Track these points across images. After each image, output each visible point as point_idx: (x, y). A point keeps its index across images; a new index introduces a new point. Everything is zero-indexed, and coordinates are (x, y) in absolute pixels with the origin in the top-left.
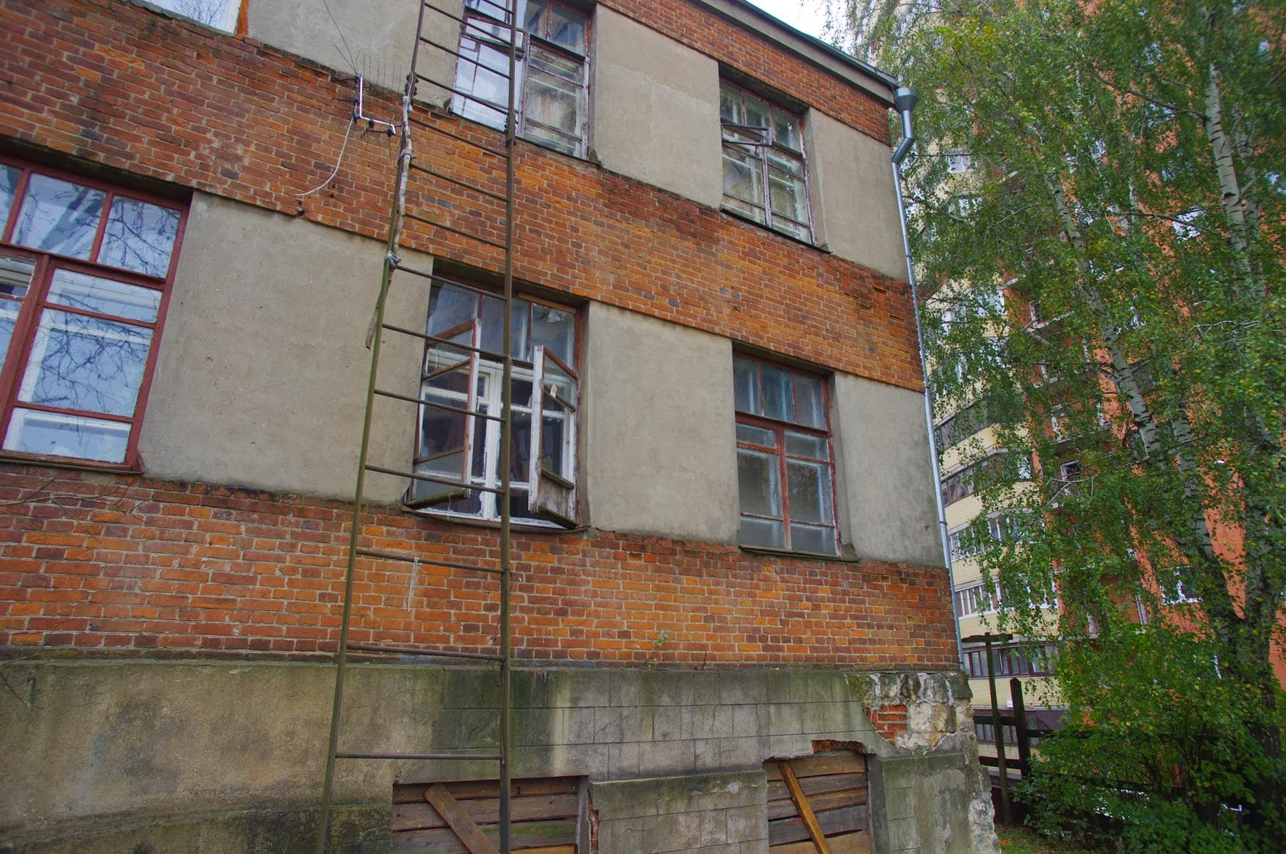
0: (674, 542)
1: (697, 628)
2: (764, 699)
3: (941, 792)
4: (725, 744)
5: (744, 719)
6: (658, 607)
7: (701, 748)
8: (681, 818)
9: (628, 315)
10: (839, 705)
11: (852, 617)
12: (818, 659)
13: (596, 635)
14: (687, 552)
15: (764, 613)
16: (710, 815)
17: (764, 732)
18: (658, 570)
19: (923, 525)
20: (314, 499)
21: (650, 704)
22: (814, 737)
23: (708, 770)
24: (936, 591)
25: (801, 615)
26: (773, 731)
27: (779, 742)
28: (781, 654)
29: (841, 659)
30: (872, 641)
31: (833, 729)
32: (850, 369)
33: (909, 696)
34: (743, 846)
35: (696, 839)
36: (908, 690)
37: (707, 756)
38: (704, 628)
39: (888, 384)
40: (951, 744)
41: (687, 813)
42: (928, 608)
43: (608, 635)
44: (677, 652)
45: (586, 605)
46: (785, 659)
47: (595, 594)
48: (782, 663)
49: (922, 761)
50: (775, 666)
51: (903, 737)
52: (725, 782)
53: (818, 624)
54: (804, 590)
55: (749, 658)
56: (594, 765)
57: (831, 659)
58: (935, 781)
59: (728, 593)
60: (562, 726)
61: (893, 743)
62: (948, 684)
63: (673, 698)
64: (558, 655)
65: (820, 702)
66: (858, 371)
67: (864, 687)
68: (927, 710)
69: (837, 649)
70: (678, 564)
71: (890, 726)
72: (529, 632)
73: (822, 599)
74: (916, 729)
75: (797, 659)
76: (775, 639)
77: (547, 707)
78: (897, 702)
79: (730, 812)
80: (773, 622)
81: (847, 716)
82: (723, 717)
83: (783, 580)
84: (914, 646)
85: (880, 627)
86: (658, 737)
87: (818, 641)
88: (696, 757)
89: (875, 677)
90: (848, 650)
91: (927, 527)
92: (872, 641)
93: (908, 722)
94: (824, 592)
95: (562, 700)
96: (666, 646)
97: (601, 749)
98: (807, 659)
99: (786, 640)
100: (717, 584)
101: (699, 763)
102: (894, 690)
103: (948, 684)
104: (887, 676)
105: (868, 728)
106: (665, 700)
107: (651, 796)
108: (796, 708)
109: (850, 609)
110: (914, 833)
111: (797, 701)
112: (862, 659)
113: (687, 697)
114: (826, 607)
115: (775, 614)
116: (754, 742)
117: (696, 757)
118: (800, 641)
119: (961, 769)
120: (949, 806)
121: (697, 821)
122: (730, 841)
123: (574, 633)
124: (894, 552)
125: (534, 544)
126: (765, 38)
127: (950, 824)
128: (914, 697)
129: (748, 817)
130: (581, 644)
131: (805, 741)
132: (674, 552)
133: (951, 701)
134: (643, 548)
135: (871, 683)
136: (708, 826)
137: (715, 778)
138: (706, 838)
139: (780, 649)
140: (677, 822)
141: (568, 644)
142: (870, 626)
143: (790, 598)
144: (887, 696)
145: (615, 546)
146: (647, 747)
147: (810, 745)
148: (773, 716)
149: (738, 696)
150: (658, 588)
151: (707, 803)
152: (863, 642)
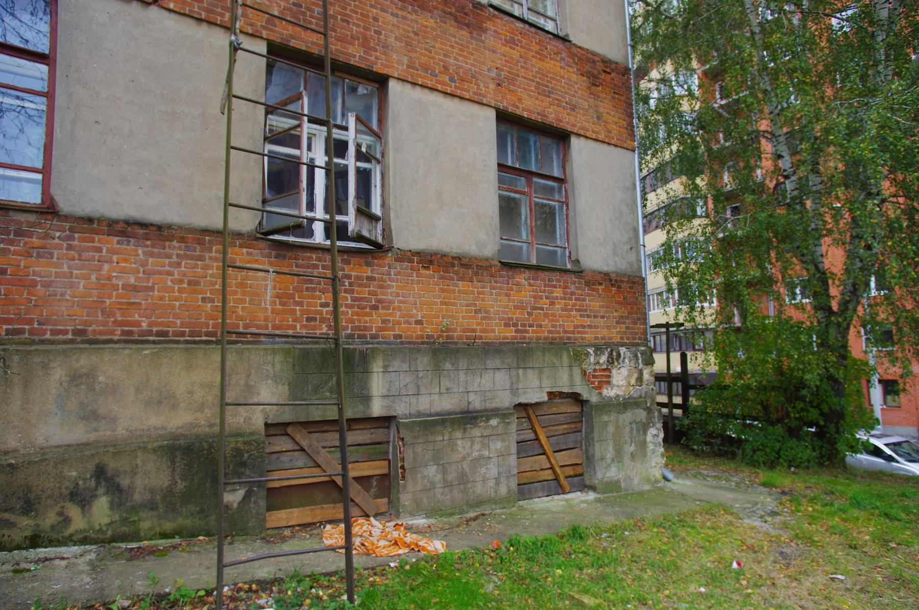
1: (470, 318)
2: (515, 365)
3: (631, 423)
4: (488, 394)
5: (502, 379)
6: (442, 303)
7: (472, 397)
8: (459, 442)
10: (566, 369)
11: (577, 310)
12: (553, 339)
13: (399, 323)
14: (462, 265)
18: (442, 278)
21: (437, 369)
25: (542, 309)
26: (521, 386)
27: (525, 393)
28: (527, 335)
29: (568, 338)
30: (590, 327)
31: (561, 384)
33: (613, 363)
34: (500, 458)
35: (469, 454)
36: (612, 359)
37: (476, 403)
42: (629, 304)
44: (455, 334)
45: (391, 302)
46: (530, 338)
48: (527, 341)
49: (619, 404)
50: (523, 343)
51: (607, 389)
52: (488, 419)
53: (553, 315)
54: (544, 291)
55: (505, 338)
56: (400, 409)
57: (561, 338)
58: (627, 416)
60: (378, 384)
61: (600, 393)
62: (639, 355)
65: (553, 366)
69: (566, 332)
70: (456, 273)
71: (599, 382)
73: (557, 298)
74: (617, 384)
75: (538, 338)
77: (367, 371)
78: (605, 367)
79: (491, 438)
80: (522, 313)
83: (530, 285)
85: (595, 317)
88: (469, 403)
89: (591, 351)
90: (573, 332)
92: (590, 327)
93: (611, 379)
94: (558, 292)
95: (377, 367)
96: (448, 330)
97: (405, 399)
98: (545, 338)
99: (531, 326)
100: (484, 287)
101: (471, 408)
102: (603, 359)
103: (639, 355)
104: (599, 350)
105: (584, 383)
107: (439, 428)
108: (536, 371)
111: (537, 366)
112: (582, 338)
113: (463, 364)
115: (523, 308)
117: (469, 403)
118: (541, 326)
119: (644, 409)
120: (635, 432)
121: (469, 444)
122: (491, 456)
123: (383, 321)
124: (608, 265)
128: (616, 364)
129: (503, 440)
131: (542, 392)
132: (453, 265)
133: (641, 366)
134: (431, 262)
135: (588, 354)
136: (477, 447)
137: (481, 417)
138: (475, 454)
139: (527, 332)
140: (456, 445)
141: (380, 329)
142: (588, 316)
143: (535, 297)
144: (598, 363)
145: (411, 261)
146: (436, 397)
149: (497, 362)
150: (443, 291)
151: (476, 432)
152: (584, 327)
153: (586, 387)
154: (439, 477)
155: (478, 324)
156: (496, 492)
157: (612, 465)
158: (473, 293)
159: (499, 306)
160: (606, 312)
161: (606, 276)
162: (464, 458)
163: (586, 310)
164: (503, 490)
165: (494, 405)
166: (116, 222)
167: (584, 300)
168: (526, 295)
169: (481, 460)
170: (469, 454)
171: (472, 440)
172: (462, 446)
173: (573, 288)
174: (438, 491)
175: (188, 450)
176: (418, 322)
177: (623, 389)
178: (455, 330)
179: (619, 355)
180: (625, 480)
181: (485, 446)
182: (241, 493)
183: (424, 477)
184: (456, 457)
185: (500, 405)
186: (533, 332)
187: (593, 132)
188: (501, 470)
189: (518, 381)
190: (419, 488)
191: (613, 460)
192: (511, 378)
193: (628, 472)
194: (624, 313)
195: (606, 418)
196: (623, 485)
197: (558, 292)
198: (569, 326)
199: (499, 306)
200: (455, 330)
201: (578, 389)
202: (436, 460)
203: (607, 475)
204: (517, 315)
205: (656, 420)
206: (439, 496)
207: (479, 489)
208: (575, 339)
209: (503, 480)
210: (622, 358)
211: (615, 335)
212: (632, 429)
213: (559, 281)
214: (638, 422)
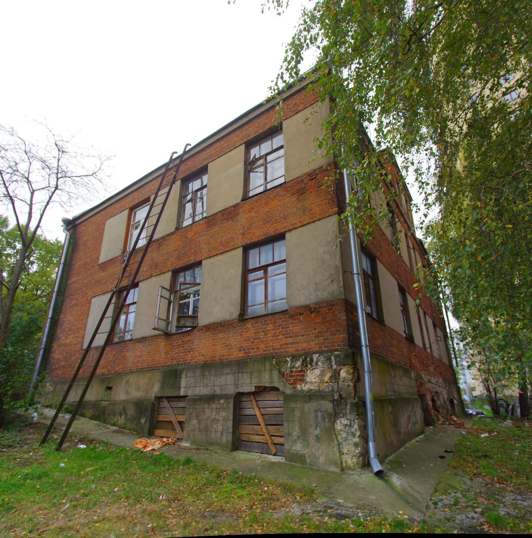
0: (218, 324)
1: (223, 350)
2: (237, 371)
3: (315, 411)
4: (223, 387)
5: (230, 378)
6: (213, 345)
7: (216, 388)
8: (207, 410)
9: (212, 258)
10: (268, 372)
11: (282, 335)
12: (265, 354)
13: (196, 356)
14: (221, 326)
15: (245, 340)
16: (214, 410)
17: (237, 383)
18: (213, 334)
19: (330, 281)
20: (149, 337)
21: (203, 375)
22: (255, 385)
23: (218, 395)
24: (334, 312)
25: (260, 338)
26: (240, 383)
27: (242, 386)
28: (250, 354)
29: (276, 353)
30: (292, 343)
32: (292, 228)
34: (224, 421)
35: (210, 417)
36: (306, 363)
37: (218, 391)
38: (224, 349)
39: (313, 222)
40: (330, 388)
41: (208, 408)
42: (327, 322)
43: (199, 356)
45: (195, 348)
46: (251, 356)
47: (197, 345)
49: (305, 396)
51: (301, 385)
53: (267, 341)
54: (261, 328)
55: (239, 357)
56: (190, 393)
57: (271, 353)
58: (312, 406)
59: (233, 336)
60: (183, 382)
61: (295, 388)
62: (333, 358)
63: (209, 373)
64: (188, 363)
66: (296, 226)
67: (282, 364)
68: (317, 372)
69: (274, 349)
70: (219, 330)
72: (182, 358)
73: (269, 330)
74: (310, 381)
75: (257, 355)
76: (248, 349)
77: (181, 377)
78: (300, 369)
80: (248, 343)
81: (271, 376)
82: (223, 378)
84: (317, 342)
85: (296, 336)
86: (205, 385)
87: (266, 347)
89: (288, 359)
90: (280, 349)
91: (332, 281)
92: (292, 343)
93: (305, 378)
94: (270, 327)
95: (183, 376)
97: (191, 388)
98: (261, 355)
99: (253, 349)
100: (230, 334)
102: (298, 364)
103: (333, 358)
104: (294, 358)
105: (280, 380)
106: (207, 373)
107: (199, 402)
108: (249, 374)
109: (282, 331)
110: (297, 428)
111: (250, 371)
112: (286, 352)
114: (270, 333)
115: (248, 340)
116: (233, 386)
117: (215, 391)
118: (258, 348)
120: (320, 418)
123: (192, 357)
124: (310, 300)
125: (185, 335)
126: (262, 113)
127: (320, 427)
128: (309, 366)
129: (226, 412)
130: (193, 360)
132: (217, 327)
133: (335, 367)
134: (209, 328)
135: (286, 361)
136: (214, 413)
138: (213, 417)
139: (250, 352)
140: (205, 411)
141: (191, 360)
142: (291, 337)
143: (255, 333)
144: (294, 367)
145: (202, 330)
146: (202, 388)
147: (254, 388)
148: (240, 377)
149: (228, 370)
150: (213, 340)
151: (214, 406)
152: (287, 344)
153: (282, 383)
154: (197, 426)
155: (226, 352)
156: (220, 440)
157: (298, 441)
158: (225, 337)
159: (237, 342)
160: (306, 331)
161: (307, 308)
162: (208, 418)
163: (290, 334)
164: (224, 440)
165: (226, 393)
166: (138, 339)
167: (288, 327)
168: (251, 334)
169: (215, 421)
170: (210, 417)
171: (212, 409)
172: (208, 412)
173: (280, 322)
174: (197, 432)
175: (135, 403)
176: (203, 355)
177: (316, 385)
178: (216, 357)
179: (312, 360)
180: (309, 456)
181: (218, 413)
182: (144, 419)
183: (192, 424)
184: (205, 417)
185: (229, 393)
186: (254, 352)
187: (299, 223)
188: (224, 428)
189: (238, 380)
190: (190, 429)
191: (299, 437)
192: (234, 378)
193: (313, 450)
194: (322, 329)
195: (293, 405)
196: (308, 460)
197: (270, 327)
198: (277, 345)
199: (237, 342)
200: (216, 357)
201: (276, 385)
202: (197, 417)
203: (294, 448)
204: (245, 345)
205: (348, 412)
206: (196, 435)
207: (213, 436)
208: (281, 353)
209: (224, 433)
210: (314, 362)
211: (314, 345)
212: (316, 417)
213: (270, 320)
214: (324, 411)
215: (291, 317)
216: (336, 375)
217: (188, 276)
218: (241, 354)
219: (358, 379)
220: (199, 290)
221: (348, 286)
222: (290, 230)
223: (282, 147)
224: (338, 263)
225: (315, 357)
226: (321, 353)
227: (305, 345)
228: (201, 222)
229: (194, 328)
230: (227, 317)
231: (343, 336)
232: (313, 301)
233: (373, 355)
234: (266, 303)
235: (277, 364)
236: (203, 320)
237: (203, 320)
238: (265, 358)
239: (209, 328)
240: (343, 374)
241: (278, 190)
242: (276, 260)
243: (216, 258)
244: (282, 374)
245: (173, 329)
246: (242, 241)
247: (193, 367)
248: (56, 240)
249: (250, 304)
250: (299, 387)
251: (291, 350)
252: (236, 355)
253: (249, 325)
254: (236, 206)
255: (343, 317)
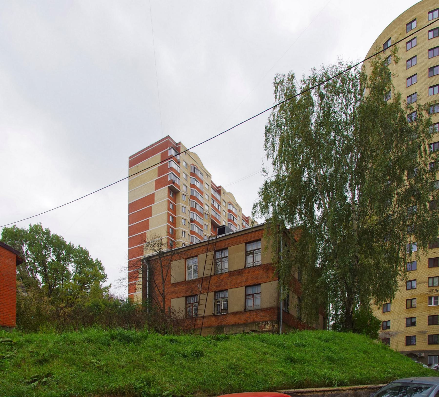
68: (269, 326)
81: (256, 327)
104: (263, 322)
149: (242, 326)
215: (262, 311)
216: (273, 326)
217: (221, 295)
218: (245, 322)
219: (279, 327)
220: (429, 343)
221: (279, 304)
222: (262, 283)
223: (260, 249)
224: (277, 296)
225: (268, 322)
226: (270, 321)
227: (266, 319)
228: (226, 273)
229: (227, 313)
230: (240, 310)
231: (276, 317)
232: (269, 307)
233: (283, 322)
234: (253, 306)
235: (257, 324)
236: (230, 310)
237: (230, 310)
238: (253, 323)
239: (233, 313)
240: (275, 326)
241: (259, 267)
242: (257, 292)
243: (234, 289)
244: (259, 327)
245: (216, 313)
246: (244, 284)
247: (229, 326)
248: (79, 246)
249: (247, 263)
250: (263, 330)
251: (261, 320)
252: (244, 322)
253: (248, 313)
254: (242, 269)
255: (277, 312)
